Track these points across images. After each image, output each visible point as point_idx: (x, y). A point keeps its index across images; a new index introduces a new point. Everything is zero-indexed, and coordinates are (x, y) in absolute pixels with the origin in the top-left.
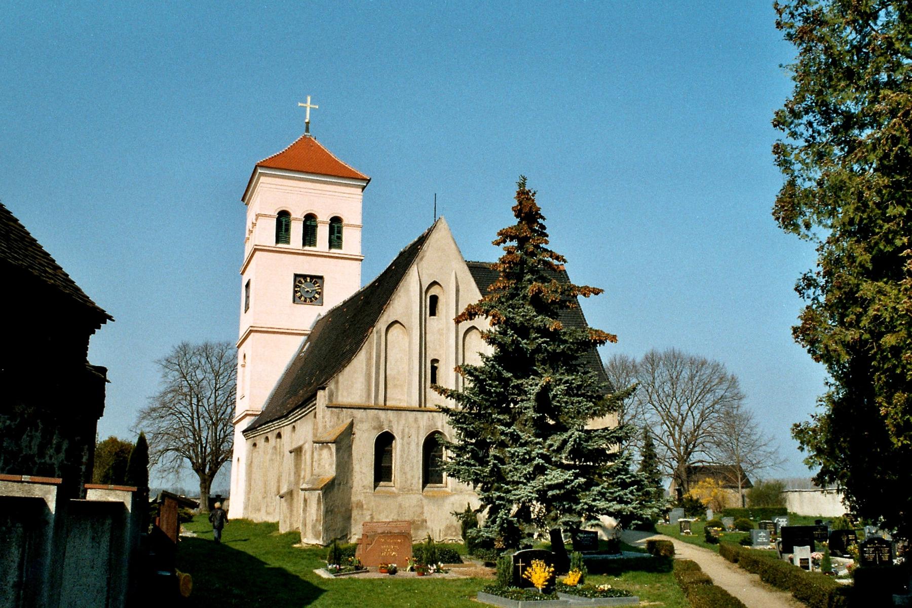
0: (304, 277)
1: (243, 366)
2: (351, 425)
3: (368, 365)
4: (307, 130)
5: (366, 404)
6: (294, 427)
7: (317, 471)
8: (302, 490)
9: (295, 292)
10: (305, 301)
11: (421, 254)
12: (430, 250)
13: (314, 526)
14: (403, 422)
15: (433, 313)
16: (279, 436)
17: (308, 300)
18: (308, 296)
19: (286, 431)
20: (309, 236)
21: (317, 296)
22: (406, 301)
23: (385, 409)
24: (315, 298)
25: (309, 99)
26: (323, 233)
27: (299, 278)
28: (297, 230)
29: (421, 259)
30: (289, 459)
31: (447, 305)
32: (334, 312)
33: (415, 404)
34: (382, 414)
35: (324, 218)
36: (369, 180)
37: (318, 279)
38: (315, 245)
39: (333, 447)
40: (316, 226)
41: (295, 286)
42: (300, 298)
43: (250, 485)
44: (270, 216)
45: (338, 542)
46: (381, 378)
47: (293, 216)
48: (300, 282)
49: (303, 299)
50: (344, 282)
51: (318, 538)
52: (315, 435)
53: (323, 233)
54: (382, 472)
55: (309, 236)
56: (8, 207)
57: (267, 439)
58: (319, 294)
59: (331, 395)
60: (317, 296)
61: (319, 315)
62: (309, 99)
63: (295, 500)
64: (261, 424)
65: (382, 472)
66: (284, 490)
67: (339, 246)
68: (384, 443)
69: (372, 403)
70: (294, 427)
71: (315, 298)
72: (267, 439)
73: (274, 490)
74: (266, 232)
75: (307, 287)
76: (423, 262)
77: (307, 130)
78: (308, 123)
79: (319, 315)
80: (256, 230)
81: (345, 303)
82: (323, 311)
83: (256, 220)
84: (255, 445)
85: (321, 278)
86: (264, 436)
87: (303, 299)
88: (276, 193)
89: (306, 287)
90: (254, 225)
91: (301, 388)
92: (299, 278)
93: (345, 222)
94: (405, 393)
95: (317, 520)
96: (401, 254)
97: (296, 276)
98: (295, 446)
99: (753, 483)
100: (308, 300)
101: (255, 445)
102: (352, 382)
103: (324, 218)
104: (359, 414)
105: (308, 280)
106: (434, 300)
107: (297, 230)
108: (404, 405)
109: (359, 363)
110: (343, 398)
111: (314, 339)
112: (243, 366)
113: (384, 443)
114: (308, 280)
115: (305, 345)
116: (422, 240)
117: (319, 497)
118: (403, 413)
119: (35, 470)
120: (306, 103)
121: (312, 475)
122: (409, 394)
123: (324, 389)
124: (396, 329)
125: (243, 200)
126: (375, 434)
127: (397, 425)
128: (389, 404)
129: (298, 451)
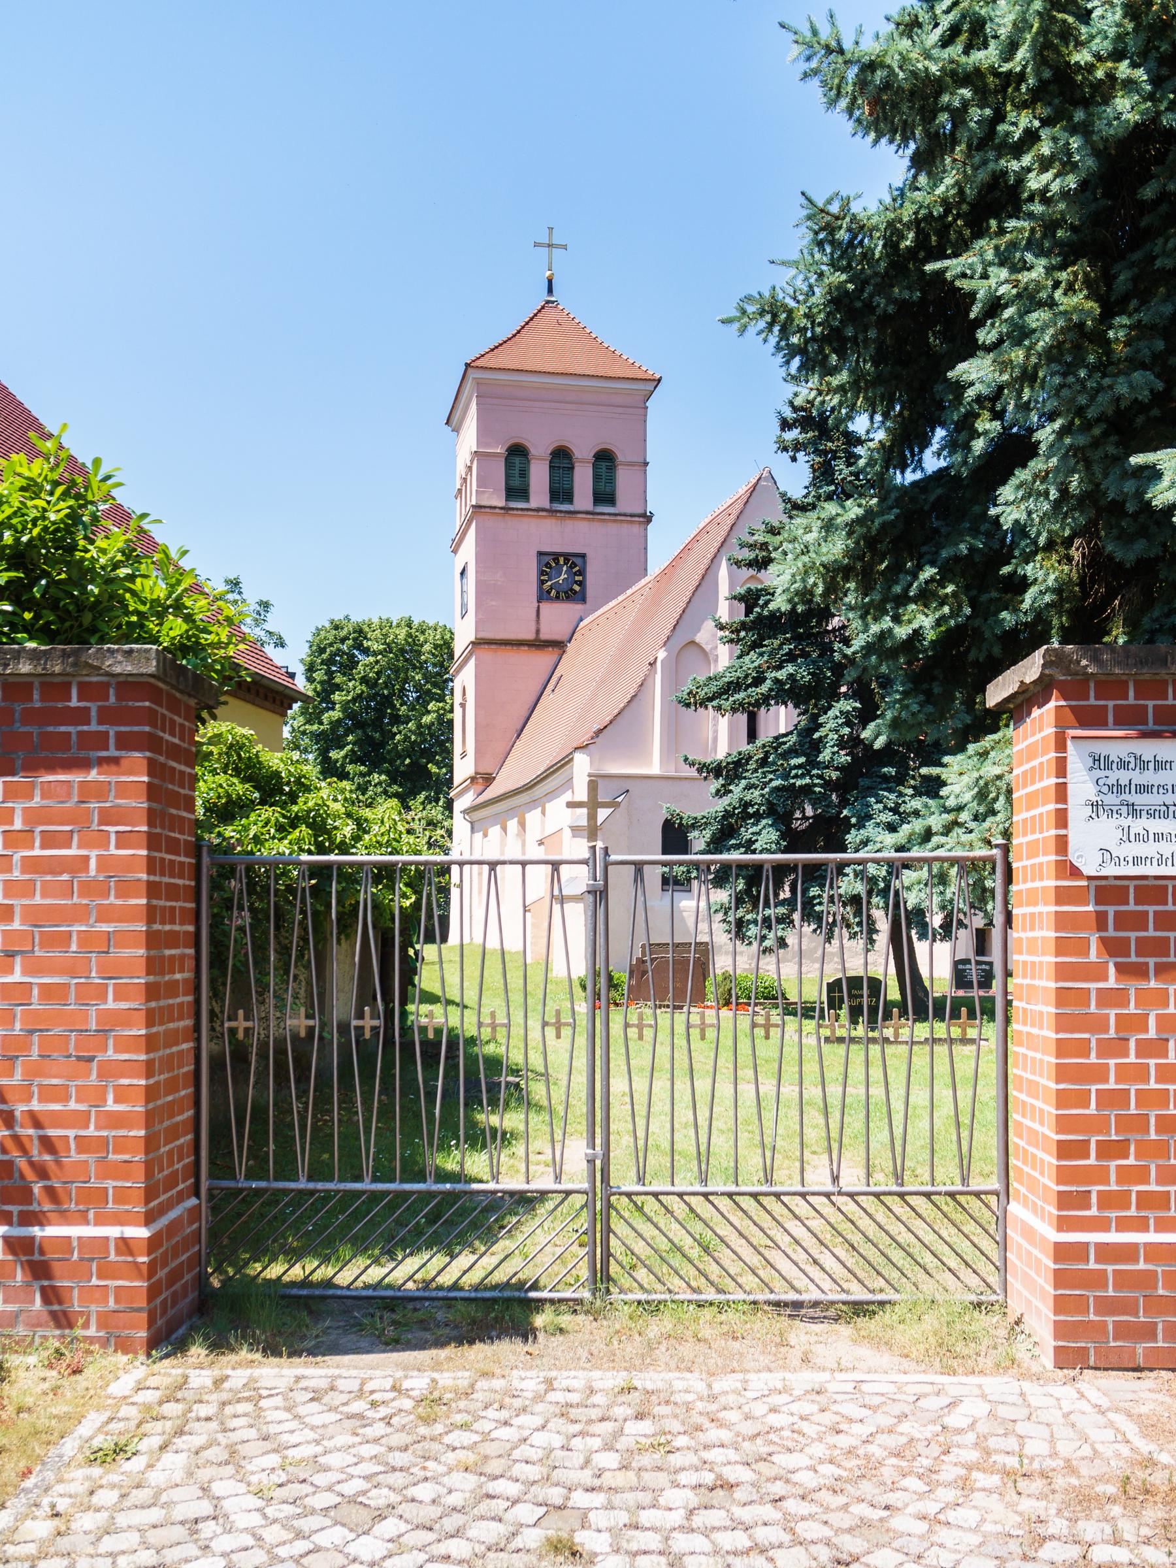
0: (556, 556)
4: (550, 291)
10: (557, 598)
17: (562, 595)
20: (561, 492)
21: (577, 588)
27: (549, 562)
35: (583, 452)
36: (659, 380)
45: (755, 1497)
47: (533, 451)
48: (548, 565)
49: (553, 593)
53: (583, 480)
55: (561, 492)
60: (577, 588)
77: (550, 291)
85: (583, 556)
87: (553, 593)
90: (470, 468)
92: (549, 562)
93: (620, 457)
97: (541, 554)
100: (562, 595)
103: (583, 452)
107: (539, 477)
118: (669, 1083)
119: (19, 763)
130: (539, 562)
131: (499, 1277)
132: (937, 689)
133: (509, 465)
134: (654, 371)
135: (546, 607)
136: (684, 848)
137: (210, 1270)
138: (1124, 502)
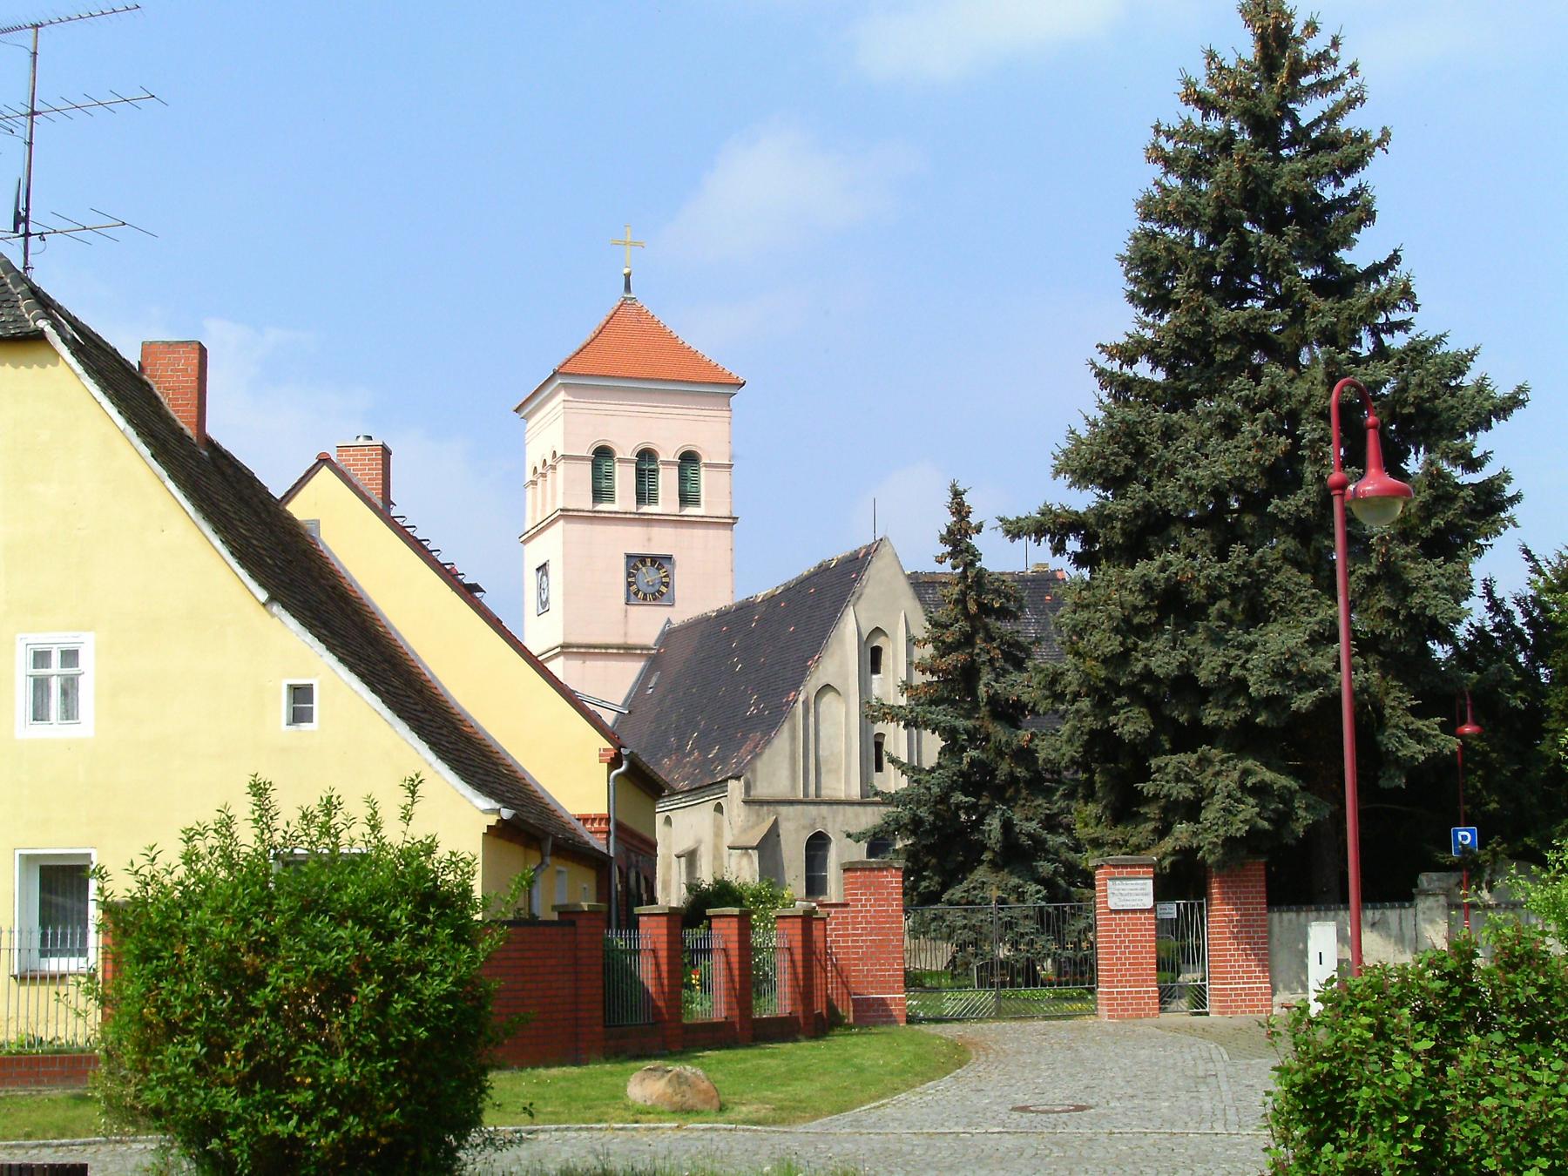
0: (643, 559)
2: (776, 822)
3: (793, 738)
4: (628, 288)
9: (629, 584)
10: (645, 599)
14: (840, 818)
15: (876, 668)
18: (652, 590)
20: (645, 494)
21: (664, 589)
24: (660, 595)
26: (667, 480)
27: (635, 562)
28: (624, 479)
31: (895, 657)
34: (812, 809)
35: (668, 453)
37: (660, 561)
38: (656, 503)
39: (755, 854)
40: (656, 471)
41: (629, 575)
42: (636, 594)
44: (582, 458)
46: (811, 762)
49: (641, 595)
50: (710, 580)
53: (667, 480)
58: (667, 585)
59: (748, 787)
60: (664, 589)
61: (669, 621)
67: (697, 502)
69: (801, 796)
71: (660, 595)
74: (573, 486)
75: (648, 576)
76: (861, 601)
77: (628, 288)
79: (669, 621)
85: (669, 558)
87: (641, 595)
89: (648, 575)
92: (635, 562)
94: (844, 780)
97: (629, 556)
98: (686, 845)
99: (1181, 979)
103: (668, 453)
104: (784, 810)
106: (876, 653)
107: (624, 479)
109: (781, 743)
110: (761, 791)
113: (817, 845)
122: (848, 782)
124: (829, 698)
127: (836, 824)
128: (826, 793)
130: (627, 563)
131: (786, 727)
132: (304, 1153)
133: (596, 467)
134: (739, 374)
135: (633, 610)
136: (1024, 901)
137: (899, 845)
138: (1415, 589)
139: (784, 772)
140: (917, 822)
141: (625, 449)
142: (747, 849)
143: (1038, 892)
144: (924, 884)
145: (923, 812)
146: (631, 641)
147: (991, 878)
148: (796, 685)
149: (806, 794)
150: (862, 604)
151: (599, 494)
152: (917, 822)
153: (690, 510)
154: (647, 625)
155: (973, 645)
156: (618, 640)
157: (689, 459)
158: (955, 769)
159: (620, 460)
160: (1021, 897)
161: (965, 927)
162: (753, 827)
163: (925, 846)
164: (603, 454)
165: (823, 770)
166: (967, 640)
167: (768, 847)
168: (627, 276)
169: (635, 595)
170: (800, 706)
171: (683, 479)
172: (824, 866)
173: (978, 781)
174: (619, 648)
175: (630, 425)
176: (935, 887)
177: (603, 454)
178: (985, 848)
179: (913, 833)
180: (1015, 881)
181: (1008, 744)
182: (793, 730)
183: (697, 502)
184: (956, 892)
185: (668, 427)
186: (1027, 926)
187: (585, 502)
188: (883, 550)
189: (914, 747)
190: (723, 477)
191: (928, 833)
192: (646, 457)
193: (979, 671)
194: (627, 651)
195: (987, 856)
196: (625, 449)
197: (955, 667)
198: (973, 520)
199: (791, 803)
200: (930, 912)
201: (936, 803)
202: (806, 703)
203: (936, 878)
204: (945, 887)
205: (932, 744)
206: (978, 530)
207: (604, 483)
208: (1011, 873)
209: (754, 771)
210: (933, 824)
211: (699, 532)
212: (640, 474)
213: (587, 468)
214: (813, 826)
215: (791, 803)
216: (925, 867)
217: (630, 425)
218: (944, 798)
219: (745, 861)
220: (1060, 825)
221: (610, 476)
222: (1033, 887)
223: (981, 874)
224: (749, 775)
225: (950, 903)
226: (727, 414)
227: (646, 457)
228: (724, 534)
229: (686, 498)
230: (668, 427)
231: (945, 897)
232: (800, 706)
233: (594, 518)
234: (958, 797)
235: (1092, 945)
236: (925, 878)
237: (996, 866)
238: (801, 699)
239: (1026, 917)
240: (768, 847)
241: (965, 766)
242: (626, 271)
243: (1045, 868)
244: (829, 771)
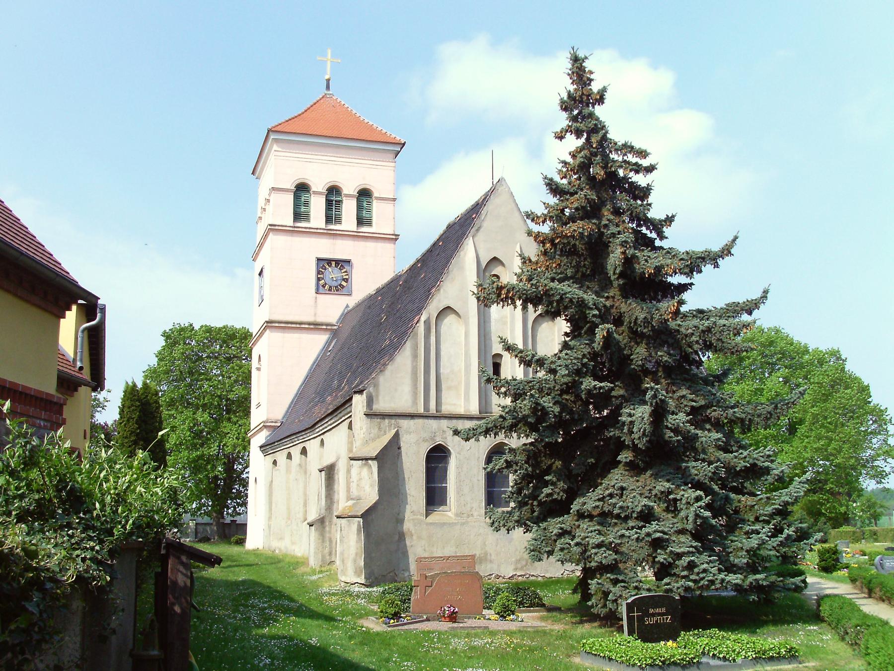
0: (329, 261)
1: (258, 369)
2: (397, 436)
3: (415, 356)
4: (328, 88)
5: (412, 411)
6: (322, 441)
7: (355, 492)
8: (338, 517)
9: (319, 279)
11: (477, 222)
12: (488, 221)
13: (355, 561)
16: (304, 452)
18: (335, 284)
19: (313, 446)
20: (332, 213)
21: (344, 283)
22: (460, 284)
23: (439, 416)
25: (329, 52)
26: (349, 208)
29: (478, 230)
30: (318, 481)
32: (371, 302)
33: (474, 409)
35: (350, 188)
36: (404, 144)
37: (342, 263)
39: (374, 465)
40: (339, 202)
41: (319, 272)
42: (324, 286)
43: (270, 509)
46: (432, 379)
50: (374, 268)
51: (359, 576)
52: (350, 450)
53: (349, 208)
54: (435, 497)
55: (332, 213)
56: (7, 204)
57: (289, 456)
58: (346, 280)
59: (370, 401)
60: (344, 283)
62: (329, 52)
63: (327, 529)
64: (282, 437)
65: (435, 497)
66: (313, 516)
67: (369, 224)
68: (437, 457)
69: (421, 410)
70: (322, 441)
71: (341, 288)
72: (289, 456)
73: (301, 516)
74: (282, 210)
75: (331, 273)
77: (328, 88)
78: (328, 80)
79: (347, 306)
80: (269, 208)
81: (379, 291)
82: (352, 301)
83: (270, 195)
84: (275, 463)
85: (348, 262)
86: (286, 451)
88: (287, 166)
89: (332, 274)
91: (327, 398)
92: (323, 263)
93: (376, 194)
95: (356, 554)
96: (450, 227)
97: (319, 260)
98: (327, 462)
101: (275, 463)
102: (396, 385)
103: (350, 188)
104: (405, 423)
105: (333, 265)
107: (317, 206)
108: (461, 411)
110: (381, 405)
111: (344, 335)
112: (258, 369)
113: (437, 457)
114: (333, 265)
115: (331, 342)
116: (477, 208)
117: (359, 525)
120: (326, 56)
121: (349, 498)
123: (360, 392)
124: (449, 320)
125: (253, 173)
126: (427, 447)
128: (446, 409)
129: (329, 471)
130: (317, 264)
131: (408, 345)
133: (297, 197)
139: (406, 388)
140: (540, 413)
141: (319, 185)
142: (367, 459)
143: (698, 499)
144: (547, 491)
145: (547, 402)
146: (320, 319)
147: (629, 482)
148: (419, 311)
149: (426, 407)
150: (480, 236)
151: (298, 216)
152: (540, 413)
153: (365, 229)
154: (332, 309)
155: (600, 218)
156: (311, 319)
157: (364, 194)
158: (587, 350)
159: (315, 193)
160: (672, 507)
161: (599, 546)
162: (374, 440)
163: (548, 445)
164: (302, 189)
165: (444, 386)
166: (591, 212)
167: (388, 458)
168: (328, 80)
169: (322, 287)
170: (421, 327)
171: (360, 208)
172: (444, 478)
173: (612, 363)
174: (309, 324)
175: (322, 169)
176: (559, 495)
177: (302, 189)
178: (620, 446)
179: (533, 428)
180: (663, 485)
181: (646, 321)
182: (415, 348)
183: (369, 224)
184: (588, 501)
185: (350, 172)
186: (683, 544)
187: (289, 220)
188: (500, 189)
189: (530, 333)
190: (388, 206)
191: (553, 428)
192: (333, 192)
193: (606, 245)
194: (315, 326)
195: (625, 456)
196: (319, 185)
197: (582, 234)
198: (595, 87)
199: (412, 416)
200: (554, 525)
201: (563, 392)
202: (427, 323)
203: (561, 484)
204: (572, 494)
205: (553, 336)
206: (601, 100)
207: (303, 209)
208: (656, 476)
209: (376, 386)
210: (559, 417)
211: (371, 245)
212: (329, 203)
213: (290, 197)
214: (433, 439)
215: (412, 416)
216: (548, 471)
217: (322, 169)
218: (572, 387)
219: (365, 471)
220: (708, 420)
221: (307, 204)
222: (692, 494)
223: (617, 478)
224: (371, 389)
225: (581, 516)
226: (393, 164)
227: (333, 192)
228: (389, 246)
229: (362, 221)
230: (350, 172)
231: (575, 507)
232: (421, 327)
233: (292, 232)
234: (588, 383)
235: (486, 509)
236: (546, 484)
237: (634, 468)
238: (423, 318)
239: (682, 532)
240: (388, 458)
241: (598, 345)
242: (327, 77)
243: (698, 469)
244: (449, 388)
